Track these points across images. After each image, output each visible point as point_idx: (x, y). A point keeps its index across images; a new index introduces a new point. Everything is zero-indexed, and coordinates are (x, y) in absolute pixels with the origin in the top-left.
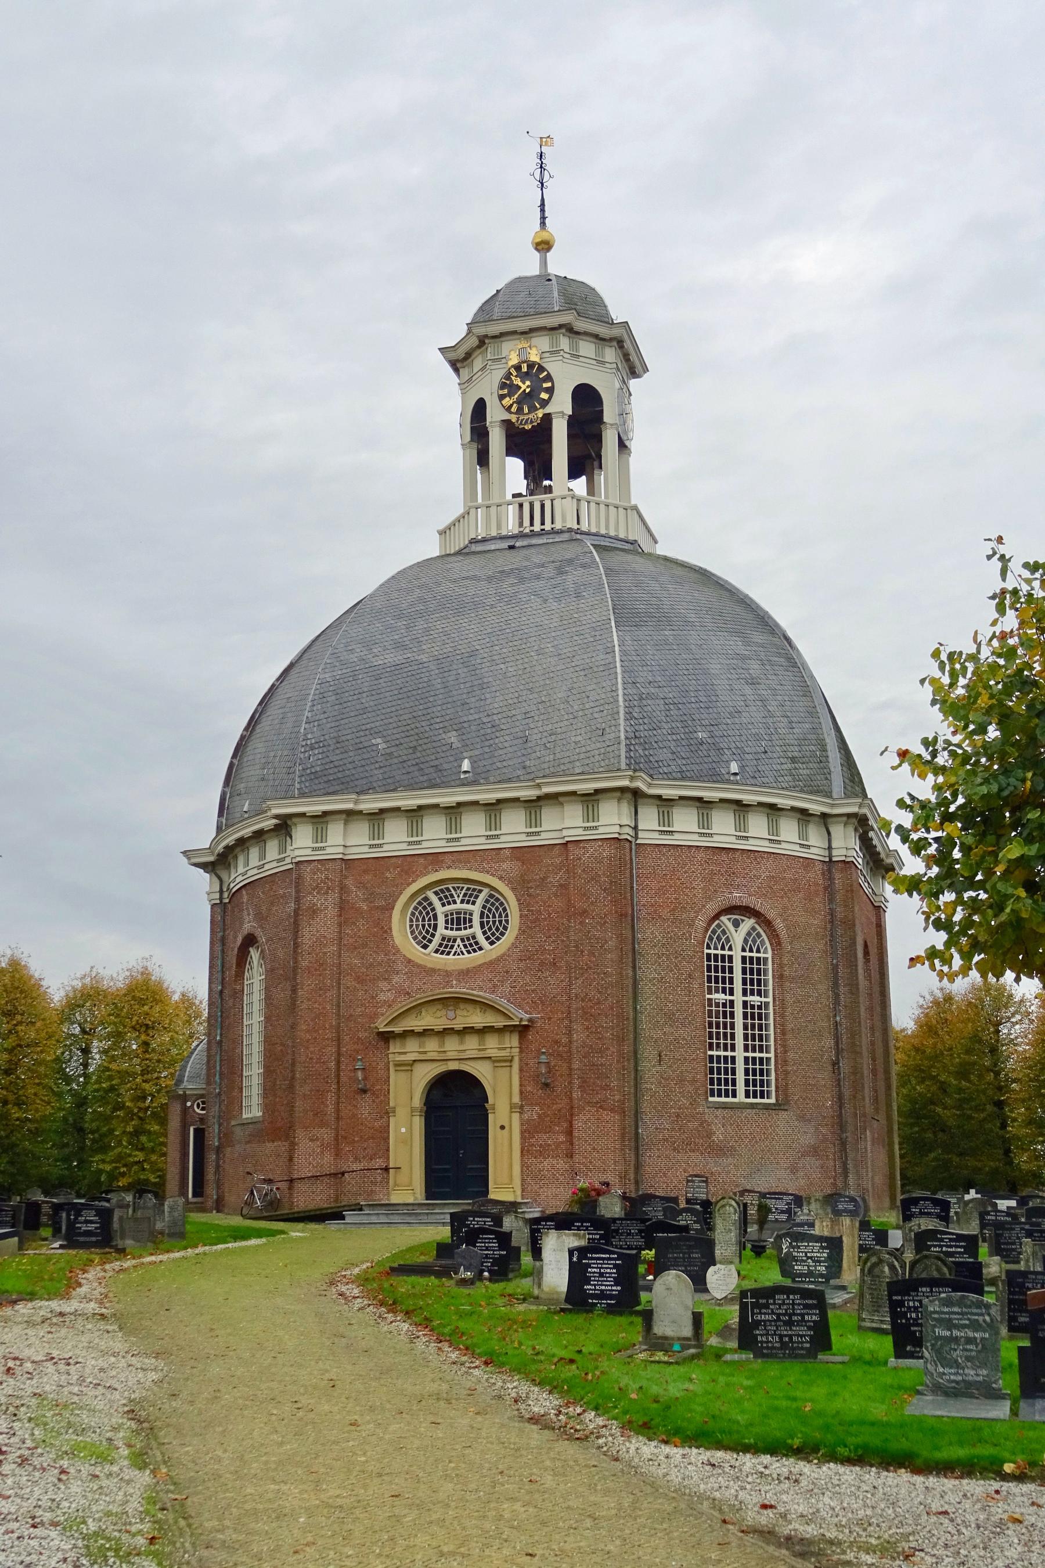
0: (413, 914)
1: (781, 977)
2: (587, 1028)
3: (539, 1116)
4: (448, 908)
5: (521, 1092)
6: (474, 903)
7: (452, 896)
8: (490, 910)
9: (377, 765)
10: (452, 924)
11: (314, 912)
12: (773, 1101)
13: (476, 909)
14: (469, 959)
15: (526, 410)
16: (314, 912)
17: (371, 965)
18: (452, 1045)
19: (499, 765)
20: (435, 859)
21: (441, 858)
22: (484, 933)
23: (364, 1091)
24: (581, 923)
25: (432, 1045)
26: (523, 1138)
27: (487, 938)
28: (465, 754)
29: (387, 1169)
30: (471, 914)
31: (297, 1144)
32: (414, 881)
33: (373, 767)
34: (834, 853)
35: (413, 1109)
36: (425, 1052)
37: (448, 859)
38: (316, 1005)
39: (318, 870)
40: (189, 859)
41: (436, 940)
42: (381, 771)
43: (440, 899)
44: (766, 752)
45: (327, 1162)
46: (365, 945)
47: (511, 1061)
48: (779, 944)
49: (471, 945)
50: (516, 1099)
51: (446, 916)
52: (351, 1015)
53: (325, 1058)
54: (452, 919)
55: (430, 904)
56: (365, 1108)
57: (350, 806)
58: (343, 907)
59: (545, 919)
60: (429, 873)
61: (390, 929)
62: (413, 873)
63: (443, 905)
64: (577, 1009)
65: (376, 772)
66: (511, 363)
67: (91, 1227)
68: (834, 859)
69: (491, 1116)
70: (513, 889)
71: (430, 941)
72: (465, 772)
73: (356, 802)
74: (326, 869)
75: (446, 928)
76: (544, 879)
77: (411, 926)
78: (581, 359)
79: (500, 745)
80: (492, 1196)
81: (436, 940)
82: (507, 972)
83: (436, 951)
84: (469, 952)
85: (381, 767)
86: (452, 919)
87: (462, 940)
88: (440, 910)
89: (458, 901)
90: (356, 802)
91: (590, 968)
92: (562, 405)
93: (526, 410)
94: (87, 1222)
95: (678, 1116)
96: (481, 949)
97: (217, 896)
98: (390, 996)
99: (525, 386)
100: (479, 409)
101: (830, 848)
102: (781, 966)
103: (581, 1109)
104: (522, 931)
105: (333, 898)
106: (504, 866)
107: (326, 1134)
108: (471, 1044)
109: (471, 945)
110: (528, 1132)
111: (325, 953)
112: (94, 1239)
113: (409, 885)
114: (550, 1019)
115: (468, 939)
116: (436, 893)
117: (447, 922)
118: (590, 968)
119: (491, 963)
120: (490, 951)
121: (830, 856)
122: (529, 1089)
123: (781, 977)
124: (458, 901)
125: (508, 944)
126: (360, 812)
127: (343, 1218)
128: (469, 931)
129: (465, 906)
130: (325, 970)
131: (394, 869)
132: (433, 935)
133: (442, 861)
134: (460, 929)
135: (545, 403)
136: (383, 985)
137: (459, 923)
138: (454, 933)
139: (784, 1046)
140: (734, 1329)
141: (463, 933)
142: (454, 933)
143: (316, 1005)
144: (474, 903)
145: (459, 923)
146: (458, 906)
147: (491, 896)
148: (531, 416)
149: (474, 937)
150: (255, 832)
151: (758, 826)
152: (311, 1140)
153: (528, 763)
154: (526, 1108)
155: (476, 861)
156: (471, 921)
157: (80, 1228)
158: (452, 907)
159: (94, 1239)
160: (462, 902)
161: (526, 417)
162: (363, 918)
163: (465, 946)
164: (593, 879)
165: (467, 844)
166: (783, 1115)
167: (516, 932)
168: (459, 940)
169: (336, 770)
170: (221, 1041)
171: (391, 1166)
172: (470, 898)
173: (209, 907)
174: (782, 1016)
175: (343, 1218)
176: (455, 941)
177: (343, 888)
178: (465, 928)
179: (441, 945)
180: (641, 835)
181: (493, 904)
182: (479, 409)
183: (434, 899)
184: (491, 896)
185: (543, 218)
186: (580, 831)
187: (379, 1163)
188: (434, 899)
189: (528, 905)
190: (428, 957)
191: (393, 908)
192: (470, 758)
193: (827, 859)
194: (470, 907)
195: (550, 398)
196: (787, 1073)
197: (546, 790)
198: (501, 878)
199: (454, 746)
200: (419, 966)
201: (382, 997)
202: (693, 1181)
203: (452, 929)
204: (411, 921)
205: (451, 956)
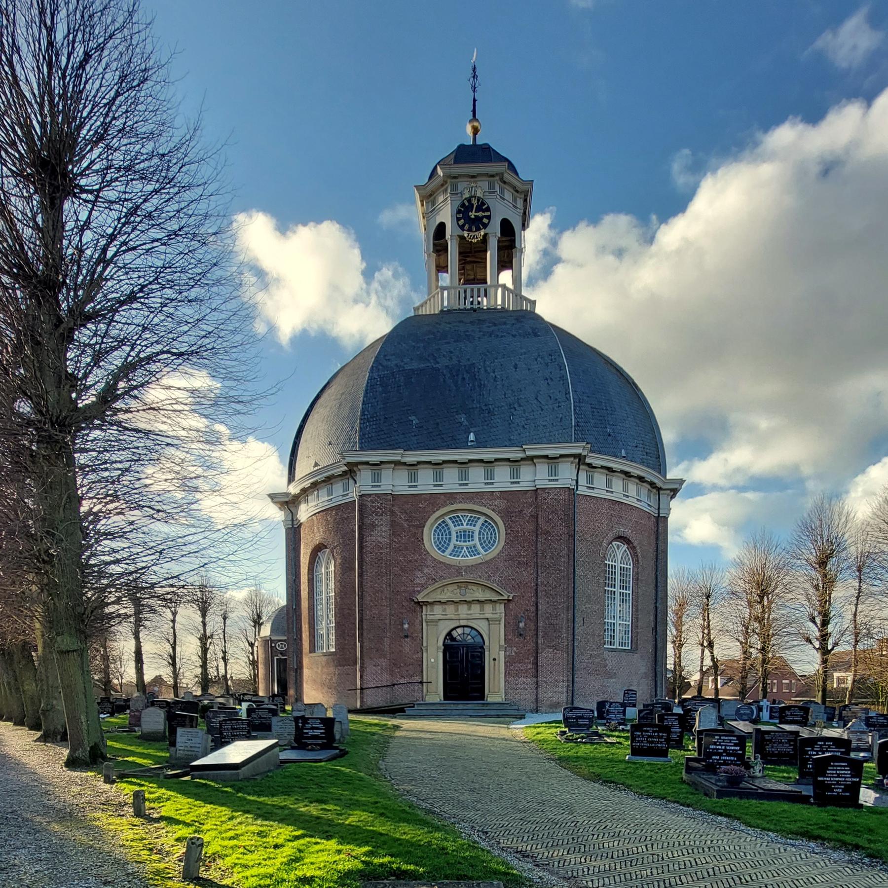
0: (435, 531)
1: (637, 579)
2: (548, 602)
3: (516, 653)
4: (458, 528)
5: (505, 639)
6: (474, 526)
7: (461, 521)
8: (445, 543)
9: (413, 434)
10: (461, 538)
11: (374, 527)
12: (629, 648)
13: (477, 529)
14: (471, 560)
15: (474, 229)
16: (373, 526)
17: (410, 561)
18: (463, 610)
19: (493, 437)
20: (451, 497)
21: (455, 496)
22: (481, 544)
23: (407, 637)
24: (545, 539)
25: (450, 609)
26: (506, 666)
27: (483, 548)
28: (471, 429)
29: (422, 683)
30: (473, 532)
31: (366, 668)
32: (437, 510)
33: (410, 435)
34: (661, 511)
35: (438, 648)
36: (446, 615)
37: (458, 496)
38: (376, 585)
39: (376, 500)
40: (272, 499)
41: (451, 547)
42: (416, 438)
43: (453, 522)
44: (636, 447)
45: (386, 679)
46: (406, 549)
47: (500, 621)
48: (638, 561)
49: (472, 551)
50: (502, 643)
51: (457, 533)
52: (398, 591)
53: (382, 618)
54: (461, 535)
55: (447, 525)
56: (407, 646)
57: (398, 458)
58: (393, 524)
59: (521, 536)
60: (447, 505)
61: (422, 539)
62: (437, 505)
63: (455, 526)
64: (542, 591)
65: (413, 438)
66: (464, 197)
67: (317, 732)
68: (661, 515)
69: (487, 653)
70: (501, 517)
71: (446, 548)
72: (472, 441)
73: (402, 456)
74: (381, 500)
75: (457, 540)
76: (521, 511)
77: (434, 538)
78: (505, 201)
79: (494, 425)
80: (490, 700)
81: (451, 547)
82: (497, 568)
83: (451, 555)
84: (471, 556)
85: (415, 436)
86: (461, 535)
87: (467, 548)
88: (453, 529)
89: (465, 524)
90: (402, 456)
91: (551, 567)
92: (494, 229)
93: (474, 229)
94: (313, 728)
95: (591, 655)
96: (479, 554)
97: (290, 523)
98: (423, 581)
99: (472, 215)
100: (441, 229)
101: (659, 508)
102: (637, 573)
103: (544, 650)
104: (506, 543)
105: (386, 519)
106: (497, 502)
107: (384, 662)
108: (476, 608)
109: (472, 551)
110: (509, 662)
111: (381, 553)
112: (320, 742)
113: (434, 512)
114: (523, 597)
115: (471, 548)
116: (450, 518)
117: (457, 537)
118: (551, 567)
119: (487, 562)
120: (484, 555)
121: (659, 514)
122: (510, 637)
123: (637, 579)
124: (465, 524)
125: (497, 551)
126: (405, 464)
127: (404, 712)
128: (471, 543)
129: (469, 527)
130: (382, 563)
131: (425, 502)
132: (448, 545)
133: (455, 498)
134: (466, 541)
135: (485, 226)
136: (419, 574)
137: (465, 538)
138: (462, 544)
139: (637, 618)
140: (326, 714)
141: (467, 543)
142: (462, 544)
143: (376, 585)
144: (474, 526)
145: (465, 538)
146: (465, 526)
147: (486, 521)
148: (476, 233)
149: (474, 547)
150: (312, 484)
151: (618, 484)
152: (375, 666)
153: (512, 437)
154: (508, 649)
155: (478, 498)
156: (472, 536)
157: (307, 733)
158: (461, 527)
159: (320, 742)
160: (467, 525)
161: (473, 234)
162: (405, 532)
163: (469, 552)
164: (553, 512)
165: (472, 488)
166: (636, 656)
167: (503, 544)
168: (465, 548)
169: (385, 436)
170: (295, 609)
171: (425, 681)
172: (472, 522)
173: (284, 530)
174: (637, 602)
175: (404, 712)
176: (462, 548)
177: (393, 513)
178: (469, 541)
179: (453, 551)
180: (580, 488)
181: (487, 527)
182: (441, 229)
183: (450, 522)
184: (486, 521)
185: (474, 111)
186: (547, 482)
187: (418, 679)
188: (450, 522)
189: (511, 527)
190: (447, 557)
191: (424, 527)
192: (474, 432)
193: (656, 515)
194: (472, 527)
195: (489, 223)
196: (638, 633)
197: (529, 453)
198: (493, 510)
199: (464, 424)
200: (441, 563)
201: (417, 581)
202: (628, 693)
203: (460, 541)
204: (434, 535)
205: (460, 558)
